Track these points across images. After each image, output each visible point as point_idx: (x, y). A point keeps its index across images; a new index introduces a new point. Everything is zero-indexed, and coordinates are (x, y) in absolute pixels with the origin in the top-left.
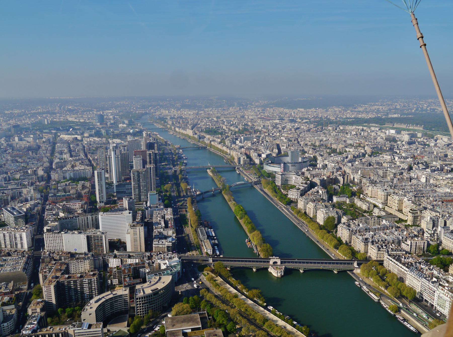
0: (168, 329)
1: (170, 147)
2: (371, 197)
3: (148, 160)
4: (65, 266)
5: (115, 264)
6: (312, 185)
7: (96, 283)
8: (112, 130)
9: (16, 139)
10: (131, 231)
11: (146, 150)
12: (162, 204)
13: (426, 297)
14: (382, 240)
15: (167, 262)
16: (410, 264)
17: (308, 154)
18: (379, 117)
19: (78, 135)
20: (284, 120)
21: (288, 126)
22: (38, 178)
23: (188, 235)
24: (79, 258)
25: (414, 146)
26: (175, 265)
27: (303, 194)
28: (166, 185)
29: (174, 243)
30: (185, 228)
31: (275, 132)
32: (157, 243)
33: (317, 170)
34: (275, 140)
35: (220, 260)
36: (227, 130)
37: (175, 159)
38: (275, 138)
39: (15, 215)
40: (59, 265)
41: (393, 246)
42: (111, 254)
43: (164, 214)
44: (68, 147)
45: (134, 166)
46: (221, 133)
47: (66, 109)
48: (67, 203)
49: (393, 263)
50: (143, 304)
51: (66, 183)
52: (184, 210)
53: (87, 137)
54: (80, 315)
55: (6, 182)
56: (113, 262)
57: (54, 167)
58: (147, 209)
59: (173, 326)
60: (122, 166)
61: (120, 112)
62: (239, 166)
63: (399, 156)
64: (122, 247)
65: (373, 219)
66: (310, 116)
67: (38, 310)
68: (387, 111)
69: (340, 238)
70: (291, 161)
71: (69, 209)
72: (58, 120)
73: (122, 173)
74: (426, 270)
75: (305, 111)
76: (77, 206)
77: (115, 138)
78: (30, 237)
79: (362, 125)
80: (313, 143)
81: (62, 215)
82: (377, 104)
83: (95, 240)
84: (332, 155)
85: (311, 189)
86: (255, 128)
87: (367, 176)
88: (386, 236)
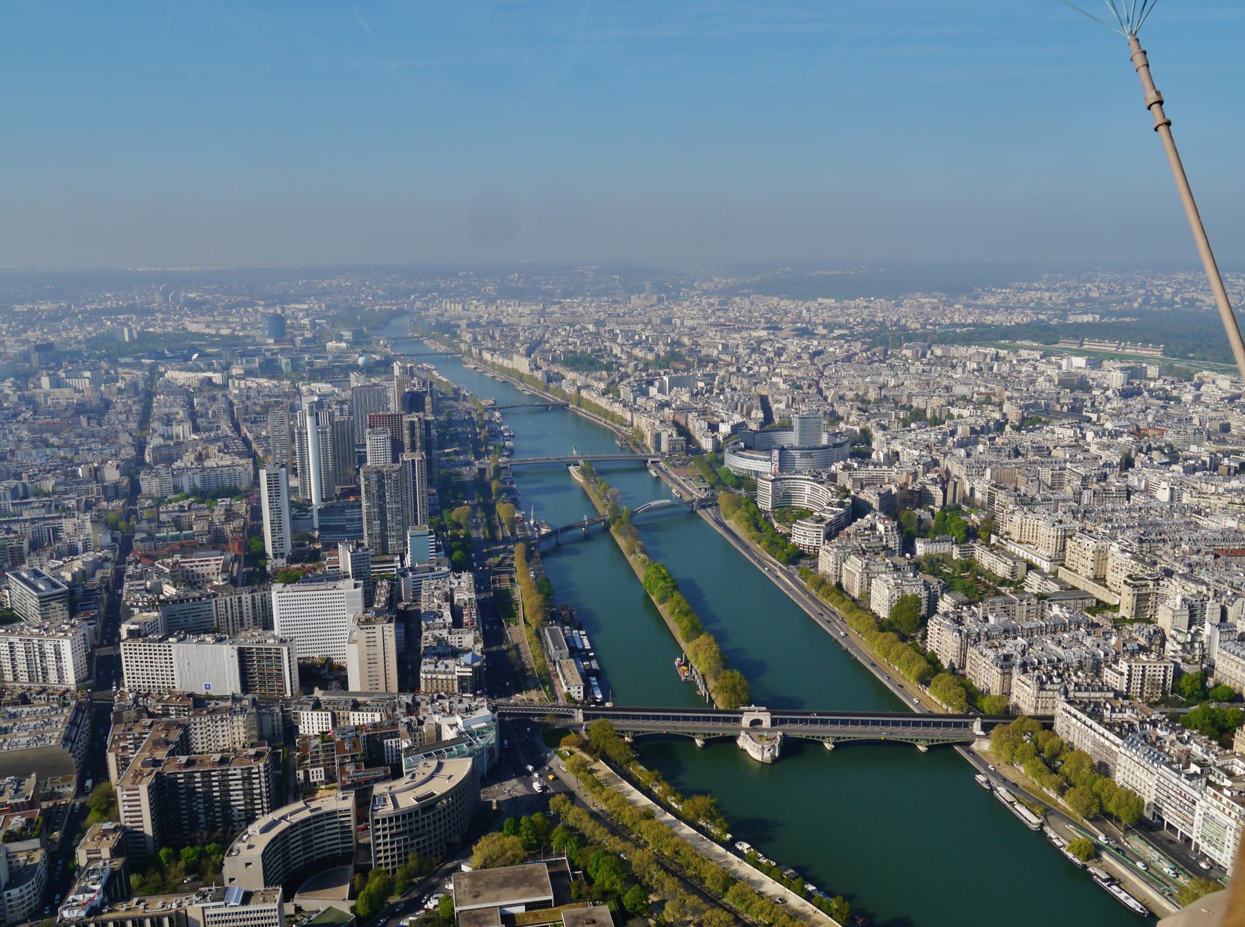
0: (461, 905)
1: (467, 405)
2: (1020, 542)
3: (407, 440)
4: (180, 731)
5: (316, 726)
6: (858, 509)
7: (263, 780)
8: (307, 357)
9: (45, 382)
10: (361, 635)
11: (403, 412)
12: (446, 560)
13: (1170, 816)
14: (1050, 661)
15: (458, 719)
16: (1126, 725)
17: (847, 423)
18: (1043, 321)
19: (215, 371)
20: (781, 329)
21: (791, 348)
22: (105, 489)
23: (516, 647)
24: (218, 709)
25: (1137, 403)
26: (482, 728)
27: (833, 533)
28: (457, 509)
29: (480, 668)
30: (509, 626)
31: (755, 363)
32: (432, 667)
33: (871, 467)
34: (756, 384)
35: (604, 716)
36: (624, 357)
37: (482, 437)
38: (756, 379)
39: (42, 591)
40: (162, 730)
41: (1079, 677)
42: (304, 698)
43: (451, 589)
44: (188, 404)
45: (368, 457)
46: (606, 366)
47: (182, 301)
48: (185, 558)
49: (1079, 724)
50: (392, 836)
51: (181, 503)
52: (507, 576)
53: (240, 378)
54: (219, 868)
55: (18, 501)
56: (310, 721)
57: (148, 459)
58: (404, 575)
59: (476, 897)
60: (334, 457)
61: (328, 308)
62: (657, 457)
63: (1096, 428)
64: (336, 678)
65: (1025, 603)
66: (851, 320)
67: (106, 853)
68: (1065, 304)
69: (934, 654)
70: (801, 443)
71: (190, 574)
72: (159, 330)
73: (336, 476)
74: (1172, 743)
75: (839, 305)
76: (211, 566)
77: (315, 380)
78: (82, 653)
79: (995, 343)
80: (860, 393)
81: (169, 590)
82: (1036, 285)
83: (260, 659)
84: (913, 425)
85: (856, 521)
86: (700, 351)
87: (1008, 485)
88: (1060, 650)
